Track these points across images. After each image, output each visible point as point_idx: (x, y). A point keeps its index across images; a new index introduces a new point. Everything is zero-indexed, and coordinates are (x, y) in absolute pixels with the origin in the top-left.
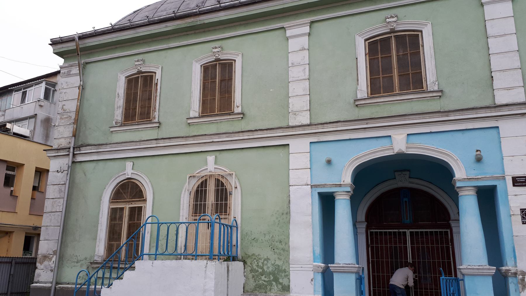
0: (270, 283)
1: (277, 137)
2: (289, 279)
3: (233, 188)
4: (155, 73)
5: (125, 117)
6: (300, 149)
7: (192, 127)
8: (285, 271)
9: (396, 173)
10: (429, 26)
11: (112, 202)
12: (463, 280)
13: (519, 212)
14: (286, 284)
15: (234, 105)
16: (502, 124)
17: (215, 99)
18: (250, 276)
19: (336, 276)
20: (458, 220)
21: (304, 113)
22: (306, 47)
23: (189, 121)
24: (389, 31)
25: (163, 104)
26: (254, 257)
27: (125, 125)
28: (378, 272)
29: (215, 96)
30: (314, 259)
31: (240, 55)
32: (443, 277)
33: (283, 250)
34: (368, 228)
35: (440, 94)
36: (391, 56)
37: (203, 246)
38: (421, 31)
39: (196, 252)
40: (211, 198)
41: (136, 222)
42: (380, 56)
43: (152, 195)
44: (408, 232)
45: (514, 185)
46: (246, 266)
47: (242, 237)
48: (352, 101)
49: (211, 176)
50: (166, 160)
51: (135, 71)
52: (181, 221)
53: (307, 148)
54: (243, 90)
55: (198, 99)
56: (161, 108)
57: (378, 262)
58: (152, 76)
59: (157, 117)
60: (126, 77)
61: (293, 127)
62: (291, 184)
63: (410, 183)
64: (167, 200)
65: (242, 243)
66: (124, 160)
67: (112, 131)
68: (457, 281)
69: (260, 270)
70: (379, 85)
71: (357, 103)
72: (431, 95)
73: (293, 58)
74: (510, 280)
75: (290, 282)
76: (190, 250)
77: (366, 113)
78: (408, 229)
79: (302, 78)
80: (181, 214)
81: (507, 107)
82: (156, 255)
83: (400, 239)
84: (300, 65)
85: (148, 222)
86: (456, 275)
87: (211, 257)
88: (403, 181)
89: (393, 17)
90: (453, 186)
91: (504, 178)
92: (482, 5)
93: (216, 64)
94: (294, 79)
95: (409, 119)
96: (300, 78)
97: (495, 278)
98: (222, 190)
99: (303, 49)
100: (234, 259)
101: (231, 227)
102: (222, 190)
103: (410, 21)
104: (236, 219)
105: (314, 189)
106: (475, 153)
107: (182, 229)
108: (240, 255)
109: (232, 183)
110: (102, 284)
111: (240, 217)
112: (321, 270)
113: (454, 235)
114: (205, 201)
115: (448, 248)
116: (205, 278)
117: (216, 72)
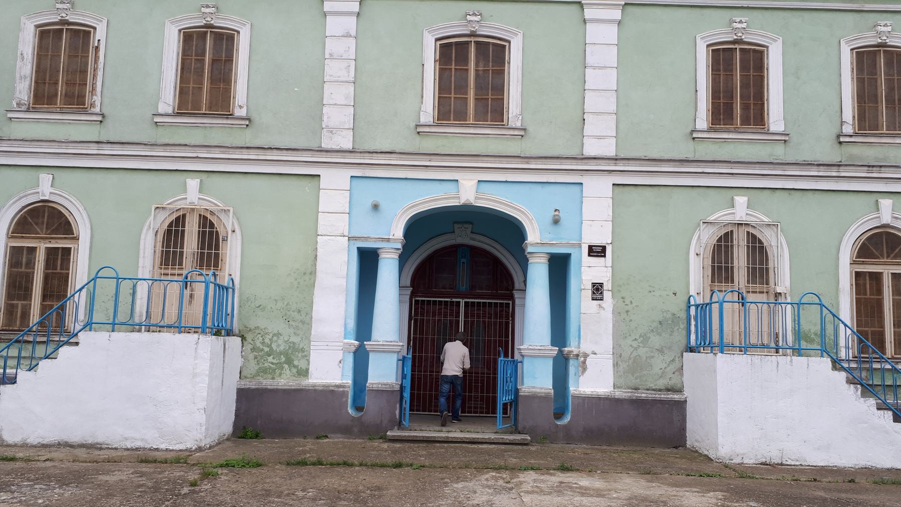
0: (280, 366)
1: (301, 162)
2: (308, 361)
3: (230, 232)
4: (95, 28)
5: (35, 96)
6: (335, 186)
7: (160, 129)
8: (303, 350)
9: (456, 226)
10: (520, 36)
11: (12, 237)
12: (521, 362)
13: (590, 287)
14: (304, 368)
15: (234, 103)
16: (586, 180)
17: (201, 89)
18: (251, 356)
19: (372, 356)
20: (524, 291)
21: (345, 133)
22: (353, 33)
23: (157, 119)
24: (468, 32)
25: (107, 83)
26: (257, 331)
27: (35, 110)
28: (421, 351)
29: (202, 84)
30: (345, 335)
31: (248, 26)
32: (502, 358)
33: (303, 322)
34: (413, 295)
35: (522, 133)
36: (467, 70)
37: (195, 313)
38: (509, 42)
39: (180, 323)
40: (191, 243)
41: (58, 271)
42: (453, 67)
43: (89, 232)
44: (462, 302)
45: (589, 255)
46: (245, 343)
47: (240, 302)
48: (413, 125)
49: (193, 210)
50: (114, 177)
51: (56, 19)
52: (140, 277)
53: (346, 184)
54: (250, 83)
55: (173, 85)
56: (105, 91)
57: (421, 340)
58: (89, 32)
59: (98, 103)
60: (37, 26)
61: (327, 151)
62: (319, 233)
63: (473, 239)
64: (112, 238)
65: (240, 313)
66: (35, 169)
67: (11, 118)
68: (515, 364)
69: (266, 349)
70: (449, 110)
71: (419, 130)
72: (512, 132)
73: (331, 46)
74: (571, 362)
75: (309, 364)
76: (122, 317)
77: (429, 145)
78: (463, 298)
79: (344, 79)
80: (141, 264)
81: (595, 161)
82: (114, 324)
83: (452, 310)
84: (341, 58)
85: (99, 275)
86: (513, 357)
87: (202, 330)
88: (463, 237)
89: (476, 15)
90: (523, 250)
91: (580, 246)
92: (585, 21)
93: (206, 33)
94: (333, 79)
95: (483, 162)
96: (341, 79)
97: (556, 360)
98: (211, 233)
99: (348, 35)
100: (229, 333)
101: (227, 289)
102: (211, 233)
103: (498, 25)
104: (233, 276)
105: (352, 242)
106: (553, 213)
107: (142, 289)
108: (236, 327)
109: (227, 224)
110: (18, 366)
111: (238, 274)
112: (354, 349)
113: (516, 308)
114: (182, 247)
115: (507, 324)
116: (196, 358)
117: (205, 45)
